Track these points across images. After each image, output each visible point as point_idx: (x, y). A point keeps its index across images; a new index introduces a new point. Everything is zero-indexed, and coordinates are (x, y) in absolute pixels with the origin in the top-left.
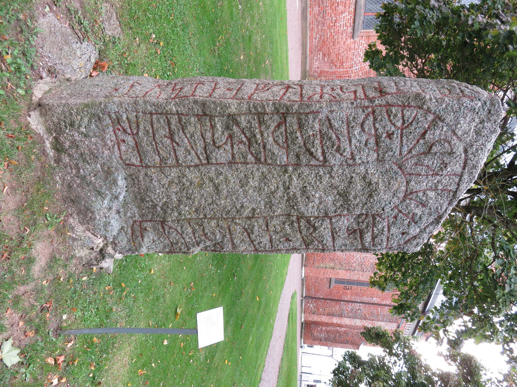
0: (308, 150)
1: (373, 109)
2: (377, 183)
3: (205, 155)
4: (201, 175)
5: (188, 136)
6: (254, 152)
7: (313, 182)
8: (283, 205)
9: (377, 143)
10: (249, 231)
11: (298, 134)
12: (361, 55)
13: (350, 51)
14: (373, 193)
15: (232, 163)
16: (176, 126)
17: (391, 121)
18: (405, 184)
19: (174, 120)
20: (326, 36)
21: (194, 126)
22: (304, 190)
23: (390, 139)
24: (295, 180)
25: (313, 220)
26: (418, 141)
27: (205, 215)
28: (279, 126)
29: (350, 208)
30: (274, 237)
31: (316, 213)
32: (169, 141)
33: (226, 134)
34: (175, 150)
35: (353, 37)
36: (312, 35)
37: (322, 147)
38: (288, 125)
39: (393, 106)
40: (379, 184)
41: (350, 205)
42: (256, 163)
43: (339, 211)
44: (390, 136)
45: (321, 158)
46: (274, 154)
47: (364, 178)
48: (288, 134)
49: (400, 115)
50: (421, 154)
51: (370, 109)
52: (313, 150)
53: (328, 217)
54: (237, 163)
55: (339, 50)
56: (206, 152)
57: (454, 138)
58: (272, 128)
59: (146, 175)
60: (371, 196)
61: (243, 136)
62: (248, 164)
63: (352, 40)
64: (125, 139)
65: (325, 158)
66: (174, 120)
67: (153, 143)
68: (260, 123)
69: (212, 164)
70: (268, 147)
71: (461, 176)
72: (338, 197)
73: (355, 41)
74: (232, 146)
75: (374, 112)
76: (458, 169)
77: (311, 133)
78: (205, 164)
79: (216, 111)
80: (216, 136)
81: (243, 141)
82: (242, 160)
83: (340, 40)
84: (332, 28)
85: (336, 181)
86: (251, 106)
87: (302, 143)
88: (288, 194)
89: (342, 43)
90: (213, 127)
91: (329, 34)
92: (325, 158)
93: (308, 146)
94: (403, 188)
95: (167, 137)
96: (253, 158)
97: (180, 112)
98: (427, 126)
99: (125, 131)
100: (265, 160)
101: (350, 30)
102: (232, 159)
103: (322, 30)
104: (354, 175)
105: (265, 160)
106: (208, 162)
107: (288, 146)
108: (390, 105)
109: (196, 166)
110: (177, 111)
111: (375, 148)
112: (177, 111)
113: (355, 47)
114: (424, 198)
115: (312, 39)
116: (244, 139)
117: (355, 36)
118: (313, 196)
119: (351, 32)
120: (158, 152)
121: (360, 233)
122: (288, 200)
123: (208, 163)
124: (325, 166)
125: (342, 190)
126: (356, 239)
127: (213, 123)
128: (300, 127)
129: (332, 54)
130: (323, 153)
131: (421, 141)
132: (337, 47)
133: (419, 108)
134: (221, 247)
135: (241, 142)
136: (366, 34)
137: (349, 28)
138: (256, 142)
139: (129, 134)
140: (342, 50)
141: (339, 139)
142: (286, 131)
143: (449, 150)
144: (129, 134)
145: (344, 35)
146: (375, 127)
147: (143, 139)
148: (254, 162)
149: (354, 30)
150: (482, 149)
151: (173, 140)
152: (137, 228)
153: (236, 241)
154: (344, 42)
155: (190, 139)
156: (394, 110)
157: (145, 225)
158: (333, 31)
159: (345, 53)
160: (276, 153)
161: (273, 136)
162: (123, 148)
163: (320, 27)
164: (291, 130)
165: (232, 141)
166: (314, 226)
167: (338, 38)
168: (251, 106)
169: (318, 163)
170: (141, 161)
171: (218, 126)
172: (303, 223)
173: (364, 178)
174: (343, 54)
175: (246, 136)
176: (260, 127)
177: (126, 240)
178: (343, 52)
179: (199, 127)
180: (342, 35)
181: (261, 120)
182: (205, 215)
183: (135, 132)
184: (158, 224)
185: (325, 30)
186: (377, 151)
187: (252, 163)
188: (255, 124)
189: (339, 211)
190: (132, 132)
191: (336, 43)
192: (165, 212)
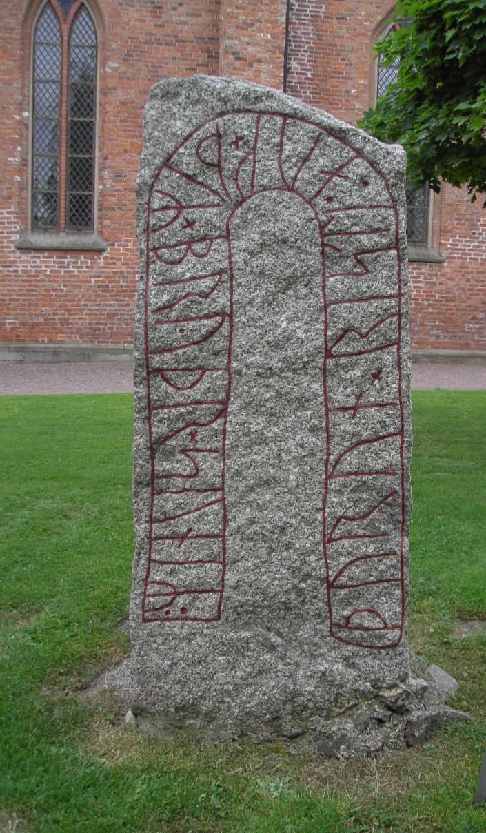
0: (205, 339)
1: (151, 250)
2: (262, 233)
3: (209, 493)
4: (242, 504)
5: (179, 512)
6: (208, 419)
7: (258, 331)
8: (305, 380)
9: (202, 240)
10: (355, 440)
11: (180, 352)
12: (476, 243)
13: (467, 268)
14: (280, 238)
15: (222, 453)
16: (166, 527)
17: (167, 225)
18: (267, 193)
19: (158, 530)
20: (434, 316)
21: (168, 503)
22: (276, 346)
23: (194, 222)
24: (253, 358)
25: (332, 331)
26: (201, 183)
27: (318, 510)
28: (167, 380)
29: (309, 272)
30: (372, 399)
31: (318, 326)
32: (186, 542)
33: (180, 456)
34: (197, 536)
35: (440, 262)
36: (430, 344)
37: (201, 318)
38: (165, 366)
39: (148, 224)
40: (264, 231)
41: (304, 274)
42: (225, 417)
43: (316, 290)
44: (190, 224)
45: (219, 319)
46: (209, 388)
47: (252, 253)
48: (181, 367)
49: (159, 214)
50: (221, 175)
51: (151, 254)
52: (203, 332)
53: (326, 306)
54: (224, 445)
55: (463, 289)
56: (206, 491)
57: (195, 136)
58: (170, 389)
59: (235, 588)
60: (284, 242)
61: (183, 432)
62: (225, 431)
63: (446, 264)
64: (180, 605)
65: (216, 314)
66: (158, 530)
67: (186, 565)
68: (162, 407)
69: (223, 483)
70: (198, 397)
71: (261, 113)
72: (290, 292)
73: (447, 258)
74: (198, 450)
75: (155, 249)
76: (244, 121)
77: (179, 334)
78: (223, 494)
79: (145, 465)
80: (181, 471)
81: (191, 434)
82: (220, 437)
83: (443, 287)
84: (419, 304)
85: (258, 295)
86: (138, 416)
87: (195, 347)
88: (282, 371)
89: (450, 284)
90: (169, 476)
91: (430, 310)
92: (216, 314)
93: (196, 338)
94: (274, 194)
95: (180, 544)
96: (218, 420)
97: (147, 519)
98: (178, 175)
99: (170, 604)
100: (219, 402)
101: (425, 269)
102: (217, 452)
103: (422, 324)
104: (248, 269)
105: (219, 402)
106: (219, 489)
107: (200, 368)
108: (147, 227)
109: (225, 507)
110: (147, 522)
111: (208, 242)
112: (147, 522)
113: (459, 258)
114: (294, 160)
115: (440, 343)
116: (188, 430)
117: (437, 257)
118: (285, 331)
119: (431, 266)
120: (199, 561)
121: (363, 252)
122: (294, 371)
123: (222, 489)
124: (232, 312)
125: (276, 286)
126: (375, 259)
127: (164, 474)
128: (170, 350)
129: (470, 302)
130: (207, 317)
131: (200, 179)
132: (457, 293)
133: (151, 189)
134: (391, 495)
135: (192, 435)
136: (436, 237)
137: (423, 271)
138: (189, 413)
139: (174, 599)
140: (463, 284)
141: (188, 294)
142: (175, 370)
143: (214, 138)
144: (174, 599)
145: (434, 280)
146: (176, 245)
147: (182, 580)
148: (223, 420)
149: (426, 262)
150: (220, 93)
151: (183, 537)
152: (343, 634)
153: (380, 465)
154: (449, 279)
155: (184, 511)
156: (152, 222)
157: (337, 617)
158: (426, 303)
159: (470, 276)
160: (209, 385)
161: (183, 389)
162: (192, 613)
163: (416, 329)
164: (173, 361)
165: (191, 450)
166: (346, 331)
167: (439, 292)
168: (138, 416)
169: (226, 325)
170: (212, 591)
171: (168, 467)
172: (340, 348)
173: (252, 253)
174: (473, 282)
175: (184, 428)
176: (168, 407)
177: (369, 660)
178: (468, 280)
179: (168, 494)
180: (434, 283)
181: (158, 403)
182: (318, 510)
183: (170, 590)
184: (335, 595)
185: (423, 317)
186: (212, 239)
187: (225, 424)
188: (163, 413)
189: (316, 290)
190: (171, 594)
191: (450, 295)
192: (309, 576)
